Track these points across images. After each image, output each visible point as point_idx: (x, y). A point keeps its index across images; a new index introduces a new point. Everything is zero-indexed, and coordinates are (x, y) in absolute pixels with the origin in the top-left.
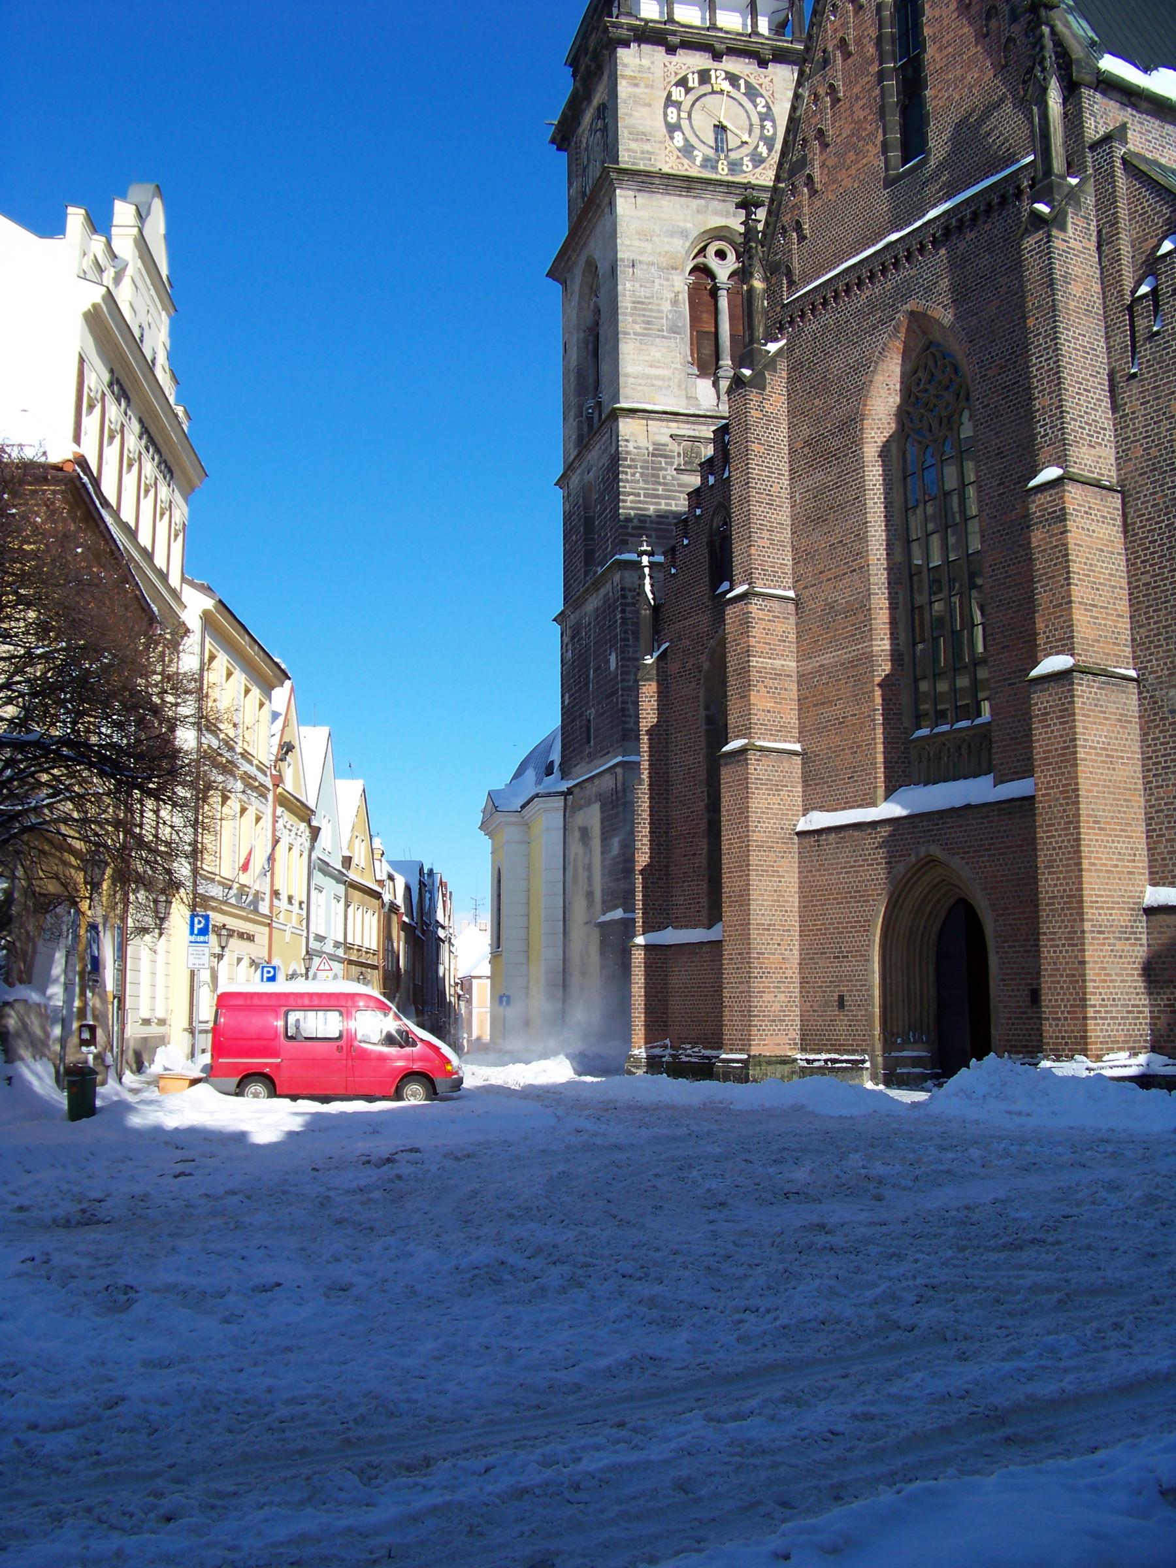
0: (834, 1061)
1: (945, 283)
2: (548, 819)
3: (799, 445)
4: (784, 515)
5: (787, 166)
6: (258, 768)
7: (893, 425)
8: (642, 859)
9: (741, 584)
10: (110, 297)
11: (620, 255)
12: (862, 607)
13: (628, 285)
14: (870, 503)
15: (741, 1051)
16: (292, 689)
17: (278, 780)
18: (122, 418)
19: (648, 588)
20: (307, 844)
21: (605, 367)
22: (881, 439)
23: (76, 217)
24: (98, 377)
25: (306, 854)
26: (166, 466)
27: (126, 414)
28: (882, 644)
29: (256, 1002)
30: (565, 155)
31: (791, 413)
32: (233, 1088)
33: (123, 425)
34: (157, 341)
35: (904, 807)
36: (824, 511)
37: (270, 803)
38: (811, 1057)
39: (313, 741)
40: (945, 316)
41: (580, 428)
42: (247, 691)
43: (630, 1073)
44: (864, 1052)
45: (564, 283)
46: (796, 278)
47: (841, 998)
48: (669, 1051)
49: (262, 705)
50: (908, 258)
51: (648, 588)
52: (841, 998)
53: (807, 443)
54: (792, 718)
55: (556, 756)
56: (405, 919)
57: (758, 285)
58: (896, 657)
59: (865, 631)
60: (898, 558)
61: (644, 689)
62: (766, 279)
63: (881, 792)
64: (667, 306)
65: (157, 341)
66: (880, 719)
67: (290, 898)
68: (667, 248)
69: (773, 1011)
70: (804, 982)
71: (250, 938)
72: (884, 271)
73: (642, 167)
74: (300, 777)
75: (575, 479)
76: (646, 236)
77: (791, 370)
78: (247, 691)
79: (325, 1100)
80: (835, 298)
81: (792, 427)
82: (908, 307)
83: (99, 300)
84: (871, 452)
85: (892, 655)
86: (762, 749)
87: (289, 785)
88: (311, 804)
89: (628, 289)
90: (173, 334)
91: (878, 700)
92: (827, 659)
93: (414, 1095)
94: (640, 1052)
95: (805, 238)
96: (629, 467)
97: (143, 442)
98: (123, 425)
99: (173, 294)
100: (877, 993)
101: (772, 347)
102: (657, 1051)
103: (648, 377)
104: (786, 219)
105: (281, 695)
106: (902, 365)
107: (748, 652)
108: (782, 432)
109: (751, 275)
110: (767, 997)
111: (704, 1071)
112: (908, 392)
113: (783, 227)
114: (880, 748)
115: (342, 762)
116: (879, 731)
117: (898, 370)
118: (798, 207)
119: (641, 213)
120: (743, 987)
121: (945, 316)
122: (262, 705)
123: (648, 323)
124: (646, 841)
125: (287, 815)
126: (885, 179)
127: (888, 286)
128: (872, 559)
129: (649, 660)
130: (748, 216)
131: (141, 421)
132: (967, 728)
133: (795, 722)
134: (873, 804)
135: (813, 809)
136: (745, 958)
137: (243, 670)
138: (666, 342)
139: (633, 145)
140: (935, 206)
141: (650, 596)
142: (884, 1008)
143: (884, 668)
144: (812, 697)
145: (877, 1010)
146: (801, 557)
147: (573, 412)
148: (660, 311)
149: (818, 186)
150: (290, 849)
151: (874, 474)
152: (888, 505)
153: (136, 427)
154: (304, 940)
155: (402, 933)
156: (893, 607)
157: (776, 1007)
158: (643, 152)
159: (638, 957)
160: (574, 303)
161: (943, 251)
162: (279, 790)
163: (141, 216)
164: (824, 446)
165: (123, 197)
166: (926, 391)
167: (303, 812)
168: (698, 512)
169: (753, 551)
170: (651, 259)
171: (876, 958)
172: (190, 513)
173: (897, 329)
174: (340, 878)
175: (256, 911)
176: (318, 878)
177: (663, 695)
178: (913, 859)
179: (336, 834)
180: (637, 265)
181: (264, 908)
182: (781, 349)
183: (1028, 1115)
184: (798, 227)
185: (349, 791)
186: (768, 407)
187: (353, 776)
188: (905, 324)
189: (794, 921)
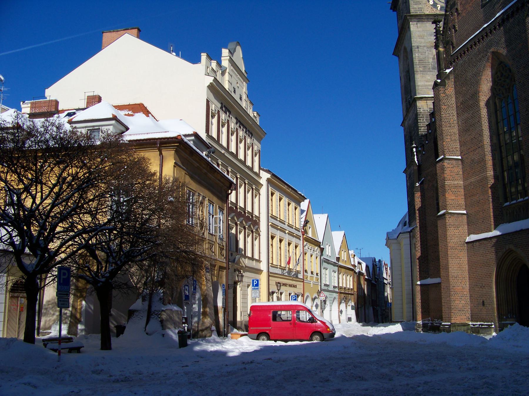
0: (482, 325)
1: (503, 40)
2: (405, 240)
3: (459, 104)
4: (456, 130)
5: (449, 6)
6: (295, 229)
7: (490, 94)
8: (419, 254)
9: (441, 155)
10: (215, 80)
11: (413, 45)
12: (483, 160)
13: (417, 55)
14: (483, 123)
15: (449, 322)
16: (309, 202)
17: (305, 232)
18: (227, 118)
19: (416, 159)
20: (319, 254)
21: (412, 84)
22: (486, 99)
23: (204, 56)
24: (215, 106)
25: (319, 258)
26: (249, 132)
27: (229, 117)
28: (490, 173)
29: (258, 309)
30: (395, 13)
31: (456, 93)
32: (256, 338)
33: (228, 121)
34: (242, 93)
35: (500, 232)
36: (469, 127)
37: (302, 241)
38: (474, 323)
39: (320, 221)
40: (503, 51)
41: (407, 106)
42: (289, 204)
43: (417, 330)
44: (492, 321)
45: (398, 57)
46: (455, 45)
47: (483, 302)
48: (430, 322)
49: (296, 209)
50: (491, 33)
51: (416, 159)
52: (483, 302)
53: (462, 103)
54: (462, 202)
55: (407, 219)
56: (366, 277)
57: (441, 49)
58: (496, 177)
59: (484, 168)
60: (495, 141)
61: (416, 195)
62: (444, 47)
63: (493, 226)
64: (431, 60)
65: (242, 93)
66: (491, 200)
67: (312, 273)
68: (430, 40)
69: (460, 308)
70: (471, 296)
71: (295, 286)
72: (483, 39)
73: (419, 13)
74: (314, 232)
75: (406, 123)
76: (421, 37)
77: (455, 78)
78: (289, 204)
79: (286, 341)
80: (468, 51)
81: (456, 98)
82: (491, 50)
83: (212, 81)
84: (482, 104)
85: (494, 177)
86: (451, 213)
87: (310, 235)
88: (320, 240)
89: (416, 56)
90: (248, 89)
91: (490, 193)
92: (473, 180)
93: (316, 339)
94: (420, 322)
95: (457, 31)
96: (421, 117)
97: (238, 125)
98: (228, 121)
99: (248, 77)
100: (495, 300)
101: (448, 71)
102: (426, 322)
103: (426, 86)
104: (450, 25)
105: (304, 205)
106: (492, 72)
107: (444, 179)
108: (453, 101)
109: (438, 46)
110: (457, 302)
111: (436, 329)
112: (494, 81)
113: (449, 28)
114: (492, 210)
115: (333, 224)
116: (491, 204)
117: (490, 73)
118: (454, 20)
119: (419, 29)
120: (448, 299)
121: (503, 51)
122: (296, 209)
123: (425, 67)
124: (419, 248)
125: (309, 244)
126: (482, 5)
127: (484, 44)
128: (485, 143)
129: (417, 185)
130: (436, 26)
131: (236, 118)
132: (522, 201)
133: (463, 203)
134: (490, 231)
135: (471, 234)
136: (448, 288)
137: (287, 197)
138: (432, 73)
139: (415, 6)
140: (499, 12)
141: (417, 162)
142: (498, 305)
143: (492, 181)
144: (468, 195)
145: (495, 306)
146: (462, 144)
147: (404, 100)
148: (429, 62)
149: (460, 12)
150: (311, 256)
151: (484, 112)
152: (490, 122)
153: (234, 120)
154: (319, 286)
155: (365, 282)
156: (494, 159)
157: (461, 305)
158: (419, 8)
159: (418, 288)
160: (402, 63)
161: (502, 28)
162: (305, 236)
163: (231, 53)
164: (467, 104)
165: (226, 48)
166: (501, 80)
167: (316, 243)
168: (430, 131)
169: (444, 143)
170: (424, 44)
171: (494, 287)
172: (261, 147)
173: (488, 59)
174: (334, 264)
175: (297, 277)
176: (325, 265)
177: (423, 197)
178: (504, 250)
179: (333, 250)
180: (419, 47)
181: (300, 276)
182: (451, 71)
183: (521, 347)
184: (454, 27)
185: (338, 236)
186: (447, 92)
187: (341, 230)
188: (491, 56)
189: (466, 274)
